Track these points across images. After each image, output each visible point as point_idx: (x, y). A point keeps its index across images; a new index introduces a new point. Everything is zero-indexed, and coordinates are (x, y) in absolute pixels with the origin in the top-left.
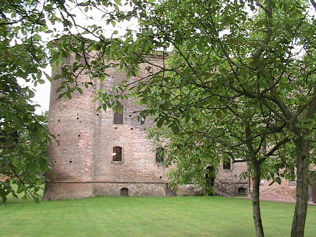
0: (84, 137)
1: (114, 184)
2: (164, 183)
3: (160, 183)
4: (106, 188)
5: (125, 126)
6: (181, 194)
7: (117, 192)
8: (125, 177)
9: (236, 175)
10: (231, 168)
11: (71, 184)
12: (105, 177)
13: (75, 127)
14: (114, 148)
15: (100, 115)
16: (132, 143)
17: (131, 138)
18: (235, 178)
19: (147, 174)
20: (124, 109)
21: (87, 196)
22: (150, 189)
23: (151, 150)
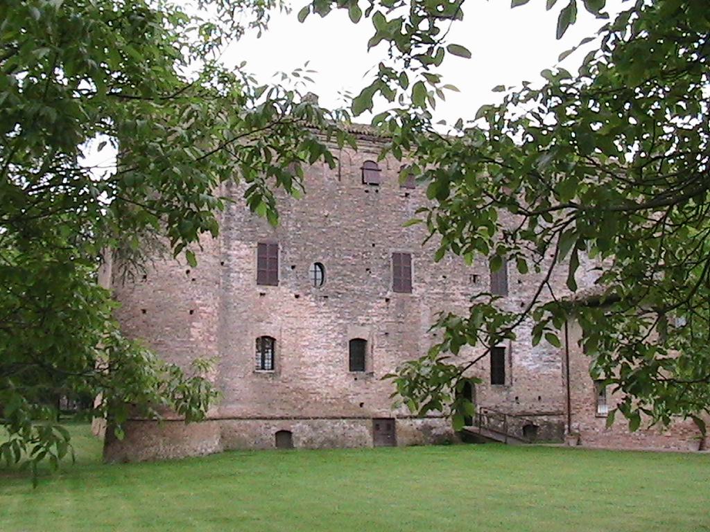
0: (202, 314)
1: (261, 422)
2: (369, 418)
3: (359, 418)
4: (244, 431)
5: (283, 289)
6: (406, 440)
7: (266, 440)
8: (284, 406)
9: (517, 398)
10: (507, 383)
11: (177, 423)
12: (240, 406)
13: (183, 293)
14: (258, 339)
15: (228, 266)
16: (299, 328)
17: (296, 317)
18: (515, 404)
19: (332, 399)
20: (279, 251)
21: (210, 451)
22: (339, 432)
23: (340, 344)
